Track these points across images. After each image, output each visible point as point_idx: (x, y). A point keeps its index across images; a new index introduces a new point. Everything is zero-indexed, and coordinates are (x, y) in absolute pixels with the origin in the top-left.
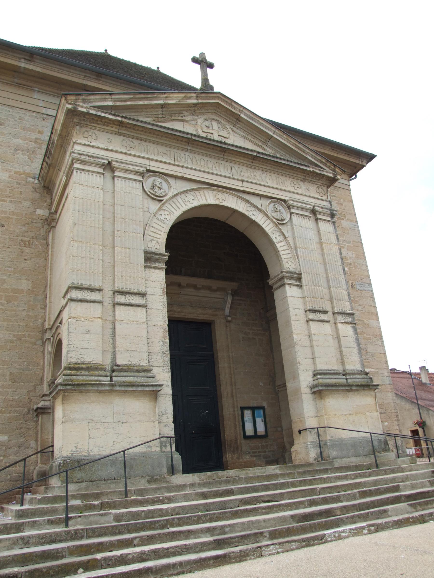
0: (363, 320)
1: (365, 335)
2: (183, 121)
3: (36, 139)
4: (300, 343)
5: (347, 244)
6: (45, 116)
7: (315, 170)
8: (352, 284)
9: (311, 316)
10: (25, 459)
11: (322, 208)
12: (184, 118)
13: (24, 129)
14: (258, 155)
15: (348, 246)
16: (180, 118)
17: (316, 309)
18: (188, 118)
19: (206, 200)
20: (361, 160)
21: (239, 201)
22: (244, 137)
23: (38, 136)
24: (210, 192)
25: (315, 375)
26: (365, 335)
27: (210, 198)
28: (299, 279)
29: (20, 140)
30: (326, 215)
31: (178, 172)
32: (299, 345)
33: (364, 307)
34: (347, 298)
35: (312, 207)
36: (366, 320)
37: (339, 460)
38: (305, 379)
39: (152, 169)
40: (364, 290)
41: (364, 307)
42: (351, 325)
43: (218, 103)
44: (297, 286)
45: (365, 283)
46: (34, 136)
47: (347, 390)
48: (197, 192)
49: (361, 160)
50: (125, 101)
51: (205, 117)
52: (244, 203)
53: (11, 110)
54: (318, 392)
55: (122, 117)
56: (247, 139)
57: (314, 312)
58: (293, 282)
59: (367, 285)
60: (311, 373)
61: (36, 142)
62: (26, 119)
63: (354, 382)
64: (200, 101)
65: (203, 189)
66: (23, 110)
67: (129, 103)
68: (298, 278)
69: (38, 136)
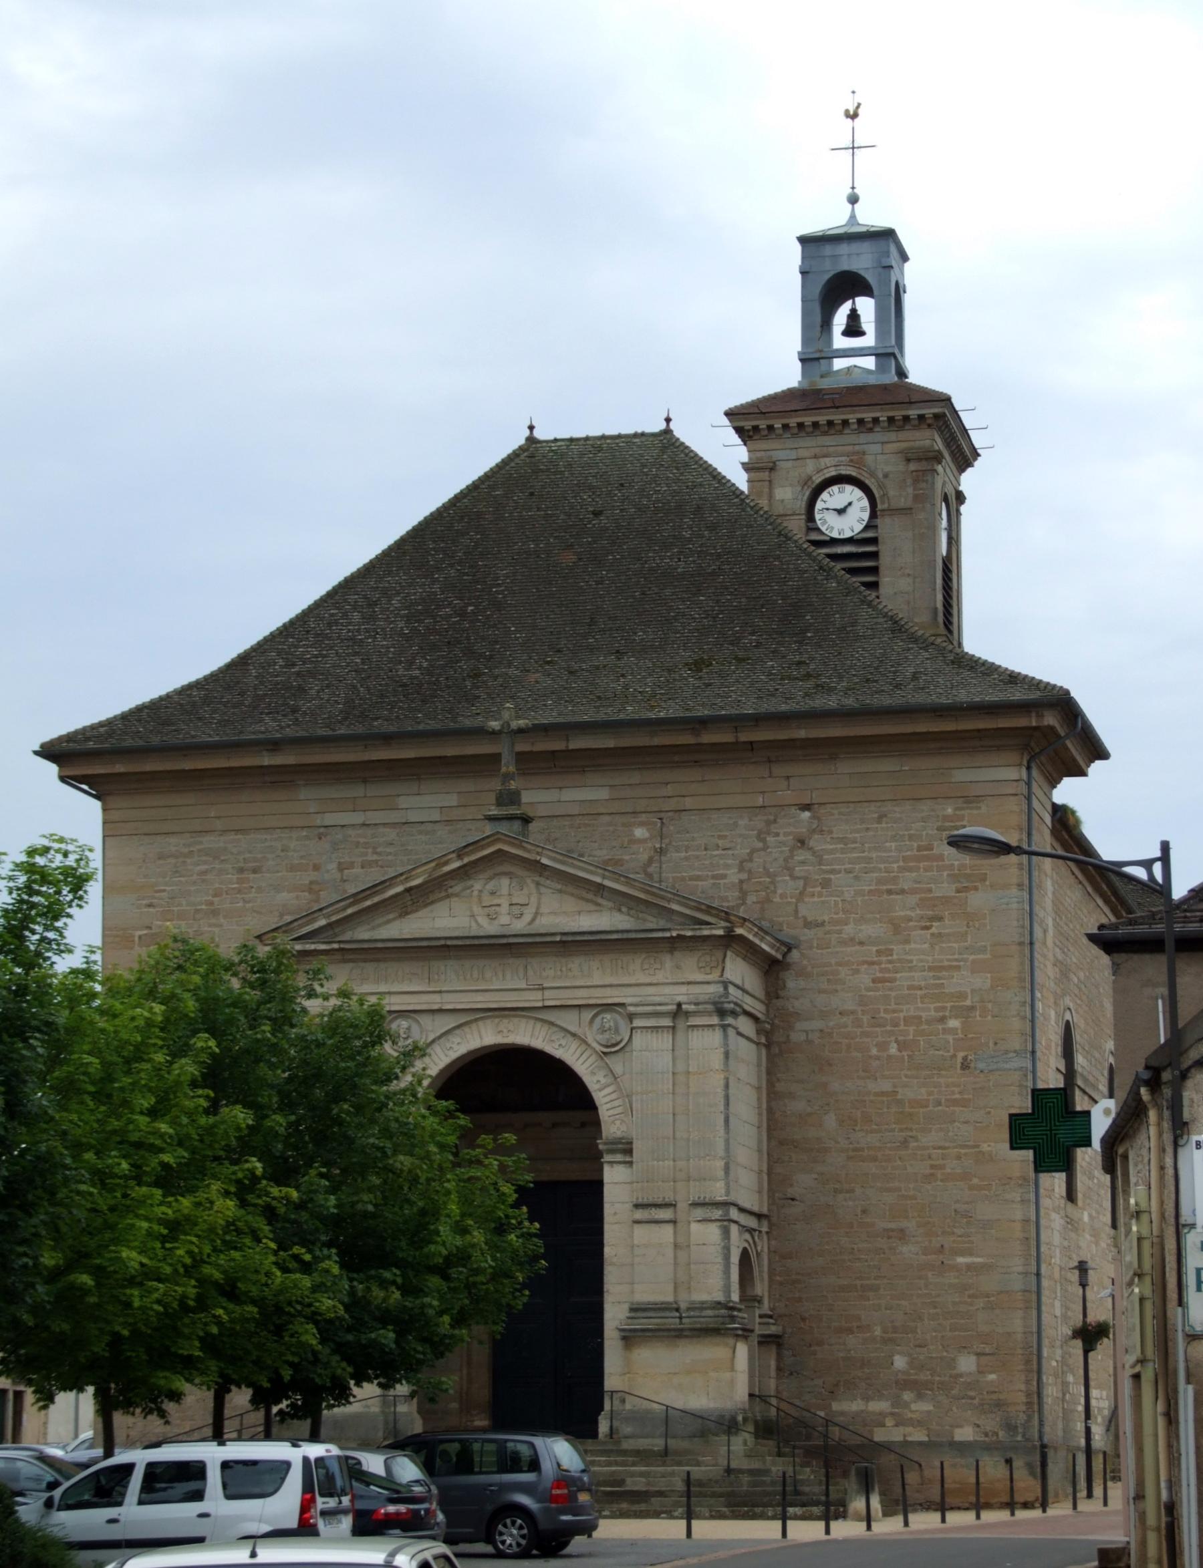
0: (978, 1146)
1: (975, 1181)
2: (448, 896)
3: (311, 883)
4: (615, 1260)
5: (972, 957)
6: (322, 830)
7: (682, 933)
8: (965, 1058)
9: (639, 1215)
10: (241, 1415)
11: (696, 1004)
12: (450, 891)
13: (292, 868)
14: (565, 938)
15: (974, 962)
16: (443, 894)
17: (651, 1201)
18: (457, 889)
19: (481, 1038)
20: (1034, 714)
21: (539, 1025)
22: (560, 891)
23: (313, 875)
24: (488, 1022)
25: (632, 1310)
26: (975, 1181)
27: (487, 1036)
28: (629, 1152)
29: (284, 894)
30: (709, 1014)
31: (435, 1001)
32: (613, 1264)
33: (989, 1113)
34: (721, 1174)
35: (675, 1007)
36: (985, 1145)
37: (631, 1441)
38: (614, 1315)
39: (393, 1008)
40: (997, 1070)
41: (989, 1113)
42: (719, 1224)
43: (500, 851)
44: (625, 1162)
45: (1007, 1052)
46: (306, 878)
47: (677, 1337)
48: (466, 1029)
49: (1034, 714)
50: (345, 909)
51: (490, 873)
52: (546, 1027)
53: (268, 837)
54: (629, 1338)
55: (339, 942)
56: (566, 893)
57: (648, 1208)
58: (619, 1157)
59: (1012, 1055)
60: (626, 1307)
61: (310, 891)
62: (292, 846)
63: (696, 1323)
64: (466, 860)
65: (476, 1020)
66: (287, 831)
67: (350, 911)
68: (626, 1148)
69: (313, 875)
